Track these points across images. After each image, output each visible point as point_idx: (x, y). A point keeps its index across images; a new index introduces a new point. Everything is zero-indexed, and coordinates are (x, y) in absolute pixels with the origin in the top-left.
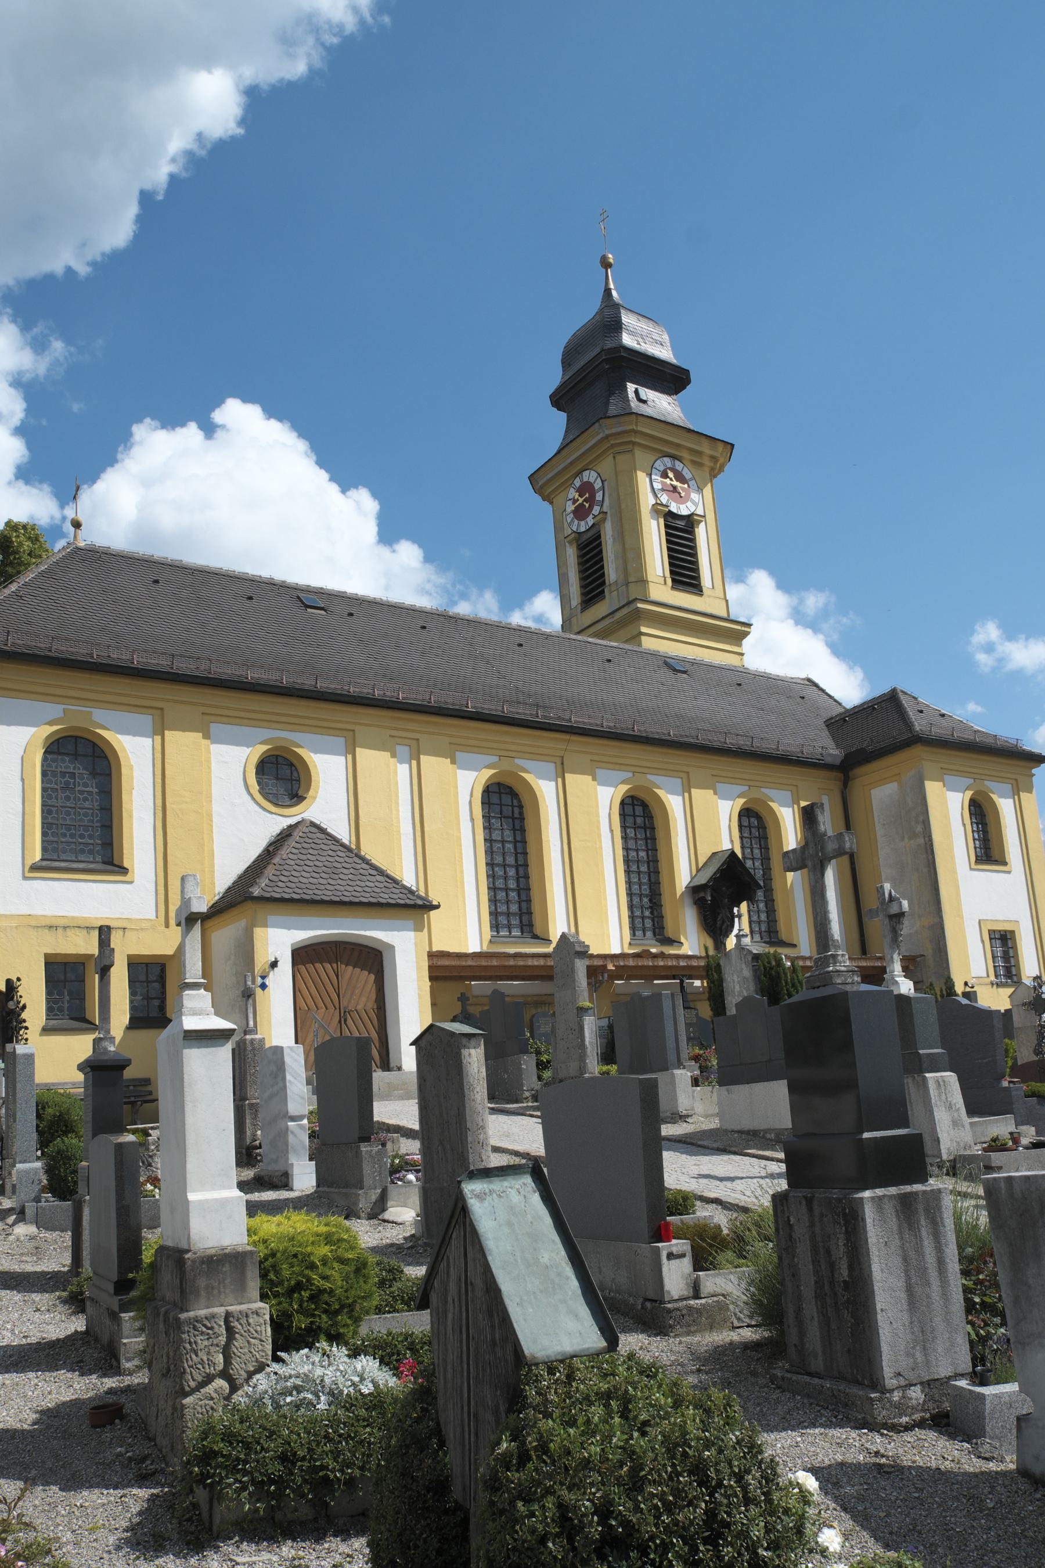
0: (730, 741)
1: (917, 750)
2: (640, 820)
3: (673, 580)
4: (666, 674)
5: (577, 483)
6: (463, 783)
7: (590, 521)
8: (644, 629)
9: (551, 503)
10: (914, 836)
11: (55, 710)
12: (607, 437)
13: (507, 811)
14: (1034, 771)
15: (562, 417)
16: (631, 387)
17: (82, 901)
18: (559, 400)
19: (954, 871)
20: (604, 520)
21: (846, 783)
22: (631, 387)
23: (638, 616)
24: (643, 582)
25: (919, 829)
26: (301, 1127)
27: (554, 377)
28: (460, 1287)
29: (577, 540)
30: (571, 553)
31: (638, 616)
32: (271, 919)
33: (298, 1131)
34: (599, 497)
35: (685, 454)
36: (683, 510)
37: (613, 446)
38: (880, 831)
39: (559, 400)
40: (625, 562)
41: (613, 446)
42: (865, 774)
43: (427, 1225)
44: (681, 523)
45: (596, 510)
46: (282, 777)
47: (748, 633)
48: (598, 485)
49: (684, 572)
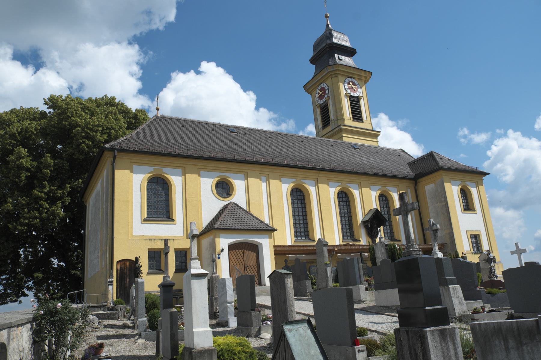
1: (441, 172)
2: (345, 199)
5: (320, 87)
6: (284, 189)
7: (324, 100)
8: (344, 135)
11: (151, 169)
12: (329, 72)
13: (299, 197)
16: (336, 56)
17: (160, 230)
20: (329, 99)
21: (416, 184)
22: (336, 56)
23: (341, 130)
24: (343, 119)
25: (443, 199)
26: (232, 305)
27: (311, 54)
30: (318, 111)
31: (341, 130)
32: (221, 235)
33: (231, 307)
34: (327, 92)
35: (356, 77)
37: (331, 75)
38: (429, 201)
39: (312, 61)
40: (336, 112)
41: (331, 75)
42: (422, 181)
44: (355, 99)
45: (326, 96)
46: (224, 188)
48: (326, 88)
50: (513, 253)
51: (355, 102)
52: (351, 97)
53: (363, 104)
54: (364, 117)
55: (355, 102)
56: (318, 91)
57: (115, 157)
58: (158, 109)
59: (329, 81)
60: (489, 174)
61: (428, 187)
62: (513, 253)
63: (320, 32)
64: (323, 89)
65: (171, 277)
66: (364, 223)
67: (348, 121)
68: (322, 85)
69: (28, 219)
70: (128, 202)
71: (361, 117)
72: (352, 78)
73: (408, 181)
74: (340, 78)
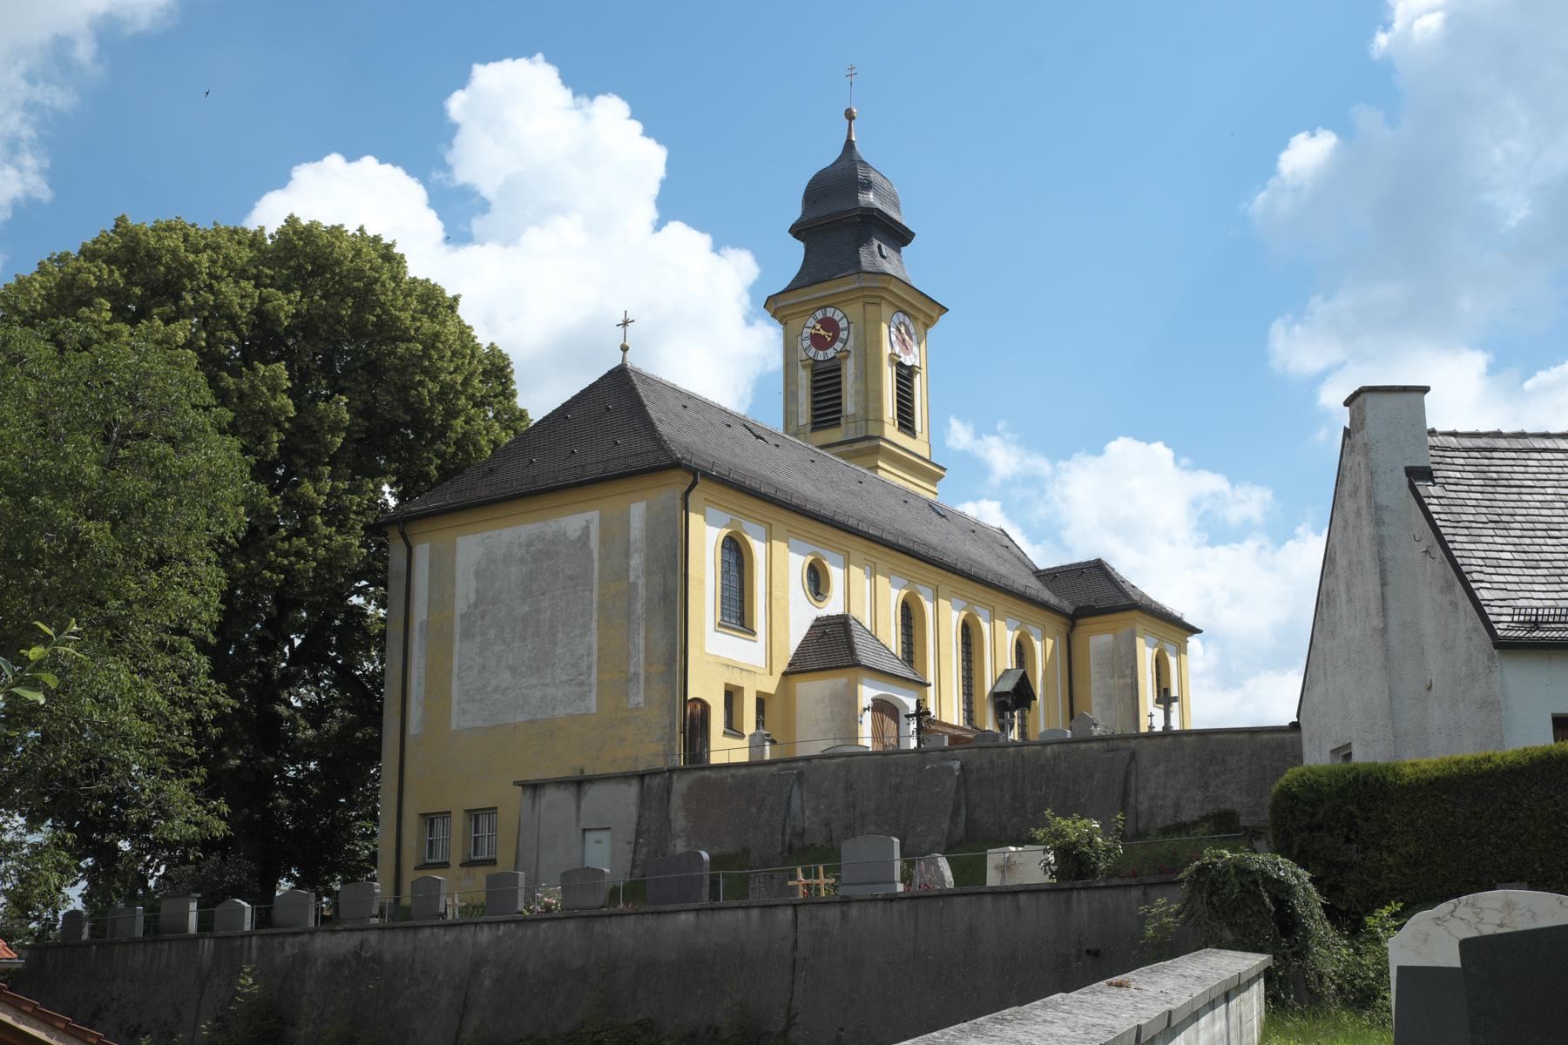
0: (982, 574)
1: (1135, 614)
2: (969, 636)
4: (927, 511)
5: (819, 315)
6: (892, 596)
7: (831, 353)
8: (880, 464)
9: (785, 324)
10: (1123, 676)
13: (910, 616)
15: (799, 247)
16: (876, 243)
18: (797, 231)
19: (703, 635)
20: (847, 357)
21: (1072, 627)
22: (876, 243)
23: (877, 451)
24: (881, 421)
25: (1128, 672)
27: (795, 212)
28: (401, 928)
29: (813, 366)
30: (804, 378)
31: (877, 451)
34: (843, 335)
35: (921, 317)
36: (908, 361)
38: (1094, 669)
39: (797, 231)
40: (866, 400)
42: (1085, 624)
43: (1512, 881)
44: (905, 372)
45: (838, 346)
47: (942, 477)
48: (843, 324)
49: (906, 421)
51: (905, 376)
52: (900, 365)
53: (918, 382)
54: (918, 427)
55: (905, 376)
56: (811, 322)
57: (694, 484)
58: (625, 349)
59: (855, 310)
61: (1098, 640)
63: (828, 155)
64: (829, 324)
65: (1100, 722)
66: (996, 695)
67: (891, 432)
68: (830, 312)
69: (286, 554)
70: (702, 582)
71: (912, 422)
72: (905, 313)
73: (1058, 618)
74: (886, 310)
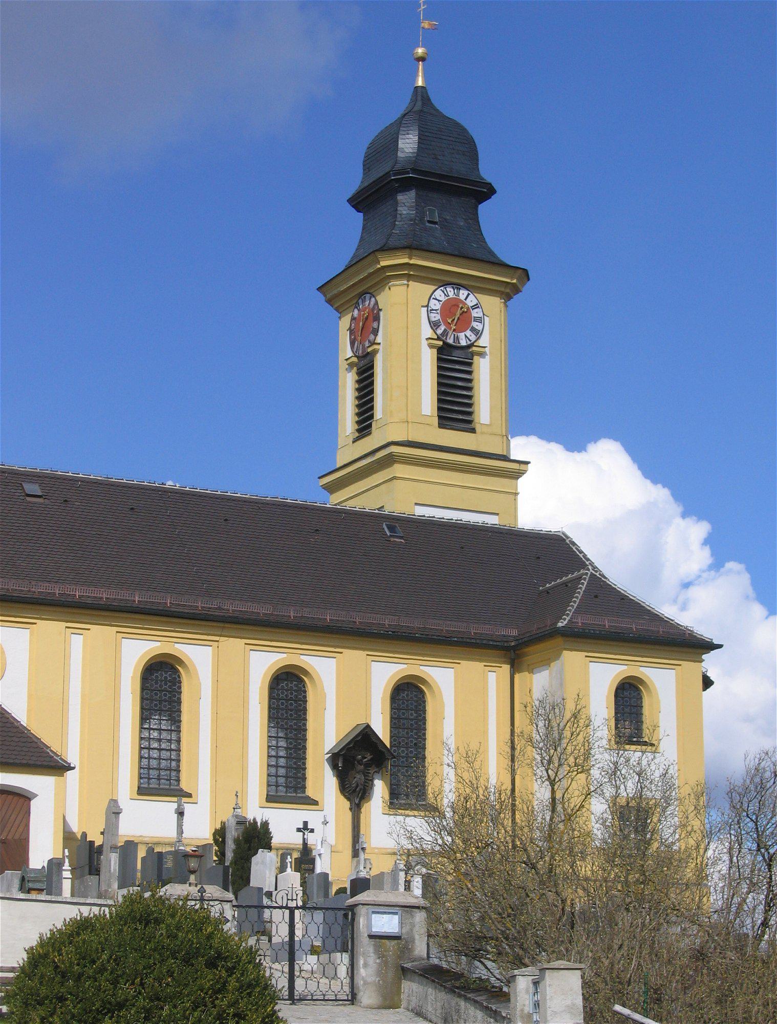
2: (288, 697)
3: (440, 417)
13: (161, 687)
14: (704, 657)
49: (455, 405)
50: (299, 830)
60: (720, 646)
62: (299, 830)
72: (458, 286)
